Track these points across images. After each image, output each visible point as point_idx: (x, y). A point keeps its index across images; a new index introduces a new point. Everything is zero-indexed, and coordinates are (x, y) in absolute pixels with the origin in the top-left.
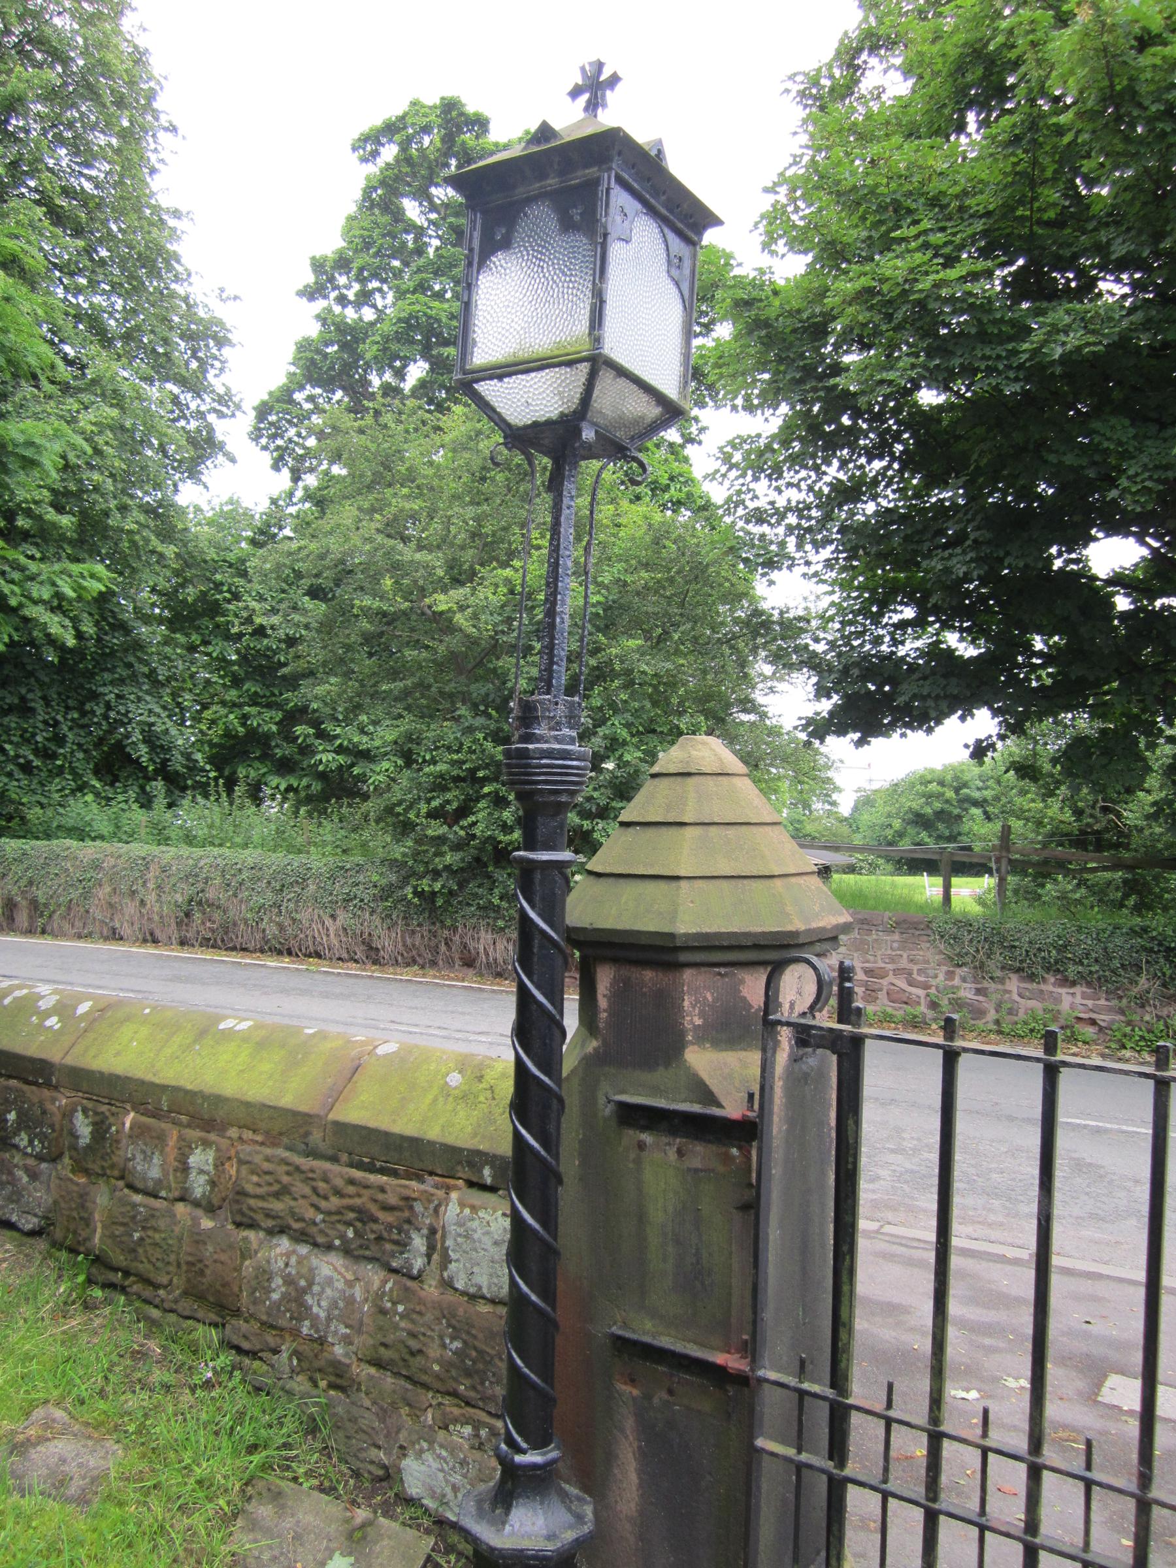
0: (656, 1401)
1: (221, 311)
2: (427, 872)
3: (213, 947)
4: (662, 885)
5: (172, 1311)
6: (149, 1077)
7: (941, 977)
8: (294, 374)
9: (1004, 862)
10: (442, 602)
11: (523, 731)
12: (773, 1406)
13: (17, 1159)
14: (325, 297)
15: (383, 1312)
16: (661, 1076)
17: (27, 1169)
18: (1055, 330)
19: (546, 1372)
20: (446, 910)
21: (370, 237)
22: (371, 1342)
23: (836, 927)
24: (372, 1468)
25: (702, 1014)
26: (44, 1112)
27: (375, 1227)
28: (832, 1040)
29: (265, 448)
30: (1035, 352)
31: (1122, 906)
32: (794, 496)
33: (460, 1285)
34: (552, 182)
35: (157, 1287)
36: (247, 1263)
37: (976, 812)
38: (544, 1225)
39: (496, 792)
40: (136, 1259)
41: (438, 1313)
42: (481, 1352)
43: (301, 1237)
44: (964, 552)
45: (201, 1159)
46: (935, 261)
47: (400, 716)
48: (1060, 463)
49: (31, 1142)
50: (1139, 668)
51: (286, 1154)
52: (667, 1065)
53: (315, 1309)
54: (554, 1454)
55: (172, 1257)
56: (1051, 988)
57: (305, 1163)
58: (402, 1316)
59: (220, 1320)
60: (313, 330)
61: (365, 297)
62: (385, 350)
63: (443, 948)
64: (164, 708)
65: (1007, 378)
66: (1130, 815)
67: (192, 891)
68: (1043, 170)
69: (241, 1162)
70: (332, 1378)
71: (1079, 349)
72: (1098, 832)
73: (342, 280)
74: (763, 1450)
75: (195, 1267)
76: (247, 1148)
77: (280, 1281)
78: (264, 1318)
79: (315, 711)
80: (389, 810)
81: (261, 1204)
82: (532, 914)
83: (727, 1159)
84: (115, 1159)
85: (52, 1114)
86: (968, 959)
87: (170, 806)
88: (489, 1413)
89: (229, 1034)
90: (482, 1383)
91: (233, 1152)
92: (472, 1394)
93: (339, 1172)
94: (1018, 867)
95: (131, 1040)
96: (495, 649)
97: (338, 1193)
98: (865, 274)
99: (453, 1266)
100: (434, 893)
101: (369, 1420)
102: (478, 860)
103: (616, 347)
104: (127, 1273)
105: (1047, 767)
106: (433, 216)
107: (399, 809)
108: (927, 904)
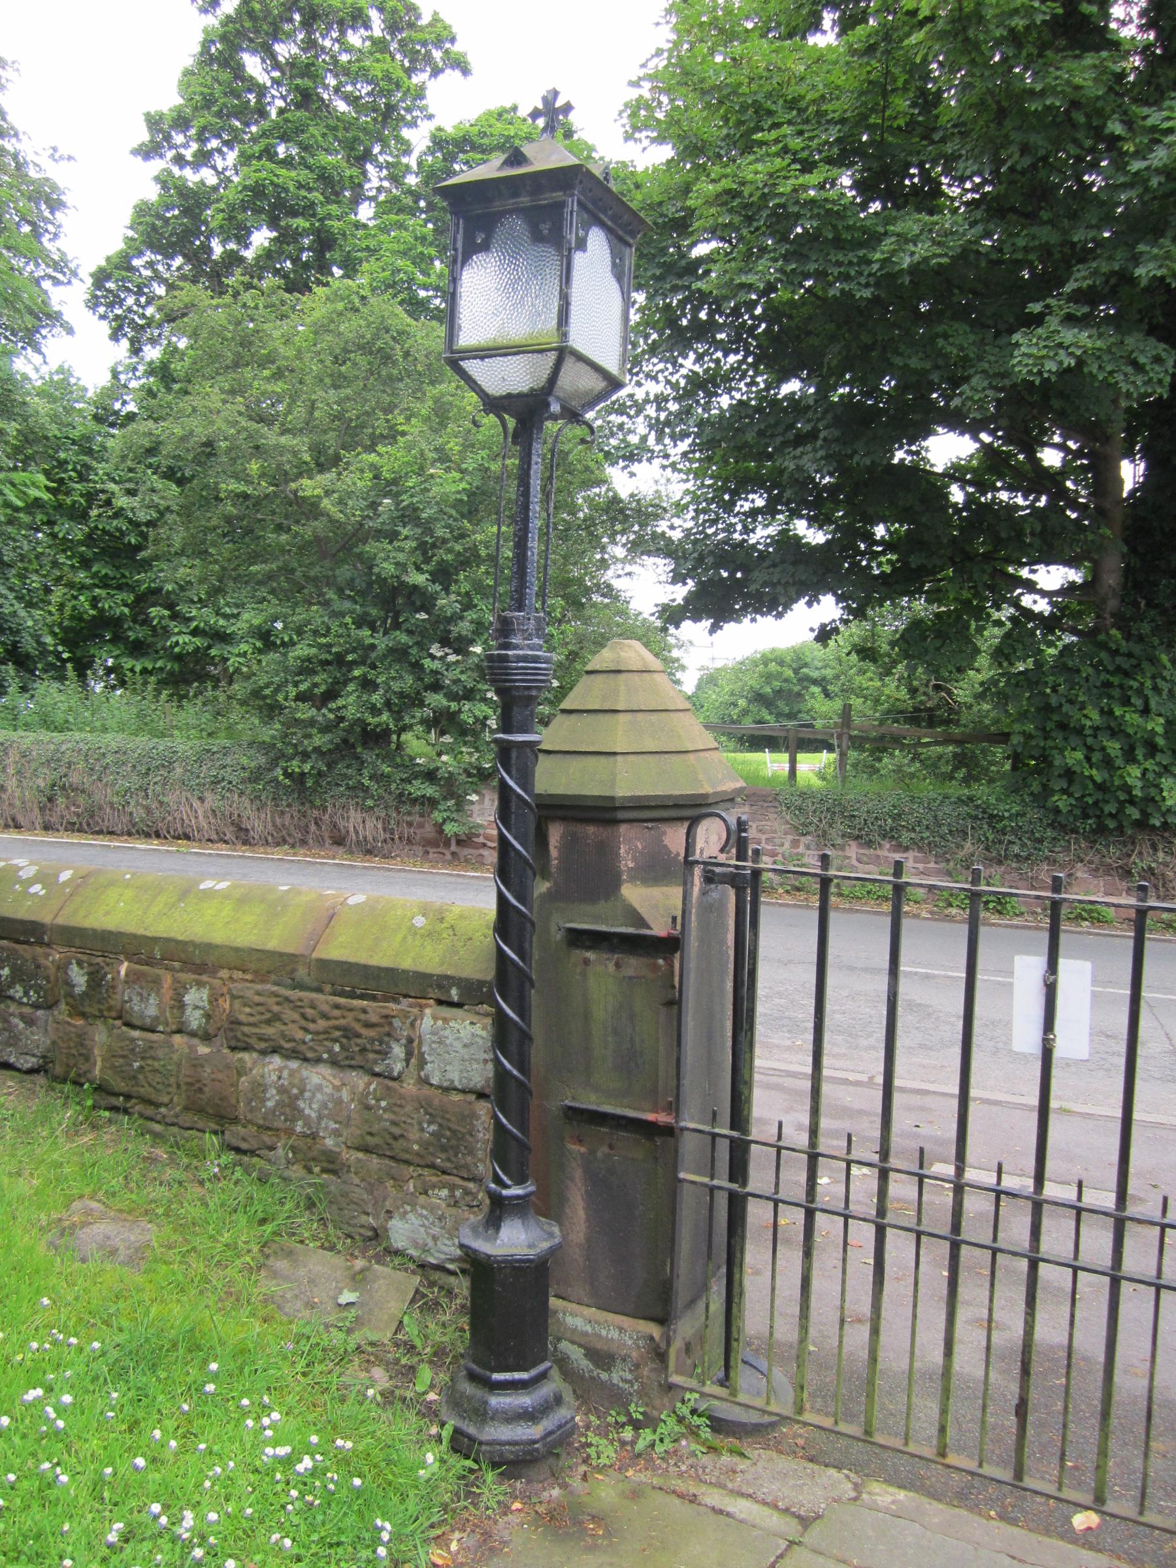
0: (599, 1154)
1: (57, 173)
2: (296, 754)
3: (79, 831)
4: (603, 760)
5: (173, 1125)
6: (141, 932)
7: (787, 845)
8: (132, 239)
9: (845, 738)
10: (309, 487)
11: (502, 640)
12: (690, 1146)
13: (13, 1008)
14: (161, 156)
15: (368, 1108)
16: (602, 907)
17: (22, 1017)
18: (903, 239)
19: (523, 1126)
20: (315, 791)
21: (211, 94)
22: (359, 1132)
23: (735, 790)
24: (362, 1231)
25: (634, 859)
26: (38, 967)
27: (359, 1041)
28: (734, 880)
29: (103, 317)
30: (885, 262)
31: (952, 778)
32: (653, 388)
33: (434, 1081)
34: (525, 200)
35: (157, 1105)
36: (243, 1079)
37: (815, 689)
38: (521, 1016)
39: (364, 675)
40: (137, 1085)
41: (416, 1105)
42: (454, 1132)
43: (294, 1054)
44: (815, 450)
45: (195, 997)
46: (793, 167)
47: (264, 599)
48: (906, 365)
49: (26, 994)
50: (969, 557)
51: (275, 988)
52: (607, 898)
53: (307, 1111)
54: (532, 1188)
55: (172, 1080)
56: (886, 853)
57: (294, 994)
58: (385, 1110)
59: (218, 1128)
60: (152, 193)
61: (203, 158)
62: (231, 218)
63: (313, 828)
64: (11, 589)
65: (859, 284)
66: (961, 692)
67: (56, 775)
68: (895, 80)
69: (234, 997)
70: (325, 1165)
71: (926, 260)
72: (931, 709)
73: (179, 139)
74: (685, 1180)
75: (194, 1085)
76: (239, 985)
77: (274, 1091)
78: (261, 1122)
79: (168, 592)
80: (257, 693)
81: (257, 1030)
82: (511, 783)
83: (655, 968)
84: (112, 1002)
85: (46, 968)
86: (812, 829)
87: (24, 689)
88: (463, 1178)
89: (209, 894)
90: (456, 1155)
91: (225, 990)
92: (448, 1165)
93: (324, 1000)
94: (858, 743)
95: (118, 902)
96: (360, 534)
97: (325, 1016)
98: (726, 176)
99: (429, 1067)
100: (303, 774)
101: (359, 1193)
102: (345, 741)
103: (578, 340)
104: (128, 1097)
105: (885, 647)
106: (276, 74)
107: (267, 692)
108: (774, 779)
